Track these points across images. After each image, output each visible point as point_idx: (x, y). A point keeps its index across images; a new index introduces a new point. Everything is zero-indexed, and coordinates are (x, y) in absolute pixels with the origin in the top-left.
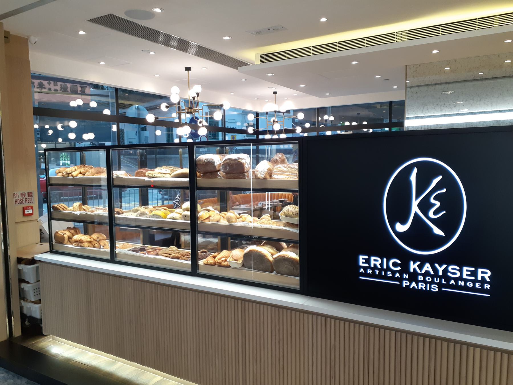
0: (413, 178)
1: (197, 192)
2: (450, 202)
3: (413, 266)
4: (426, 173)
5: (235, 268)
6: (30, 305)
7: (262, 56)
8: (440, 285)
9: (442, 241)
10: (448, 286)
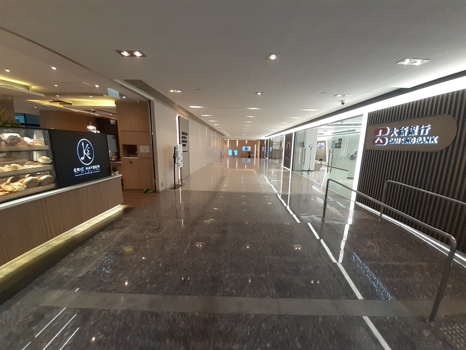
0: (83, 144)
3: (87, 168)
5: (21, 191)
9: (91, 160)
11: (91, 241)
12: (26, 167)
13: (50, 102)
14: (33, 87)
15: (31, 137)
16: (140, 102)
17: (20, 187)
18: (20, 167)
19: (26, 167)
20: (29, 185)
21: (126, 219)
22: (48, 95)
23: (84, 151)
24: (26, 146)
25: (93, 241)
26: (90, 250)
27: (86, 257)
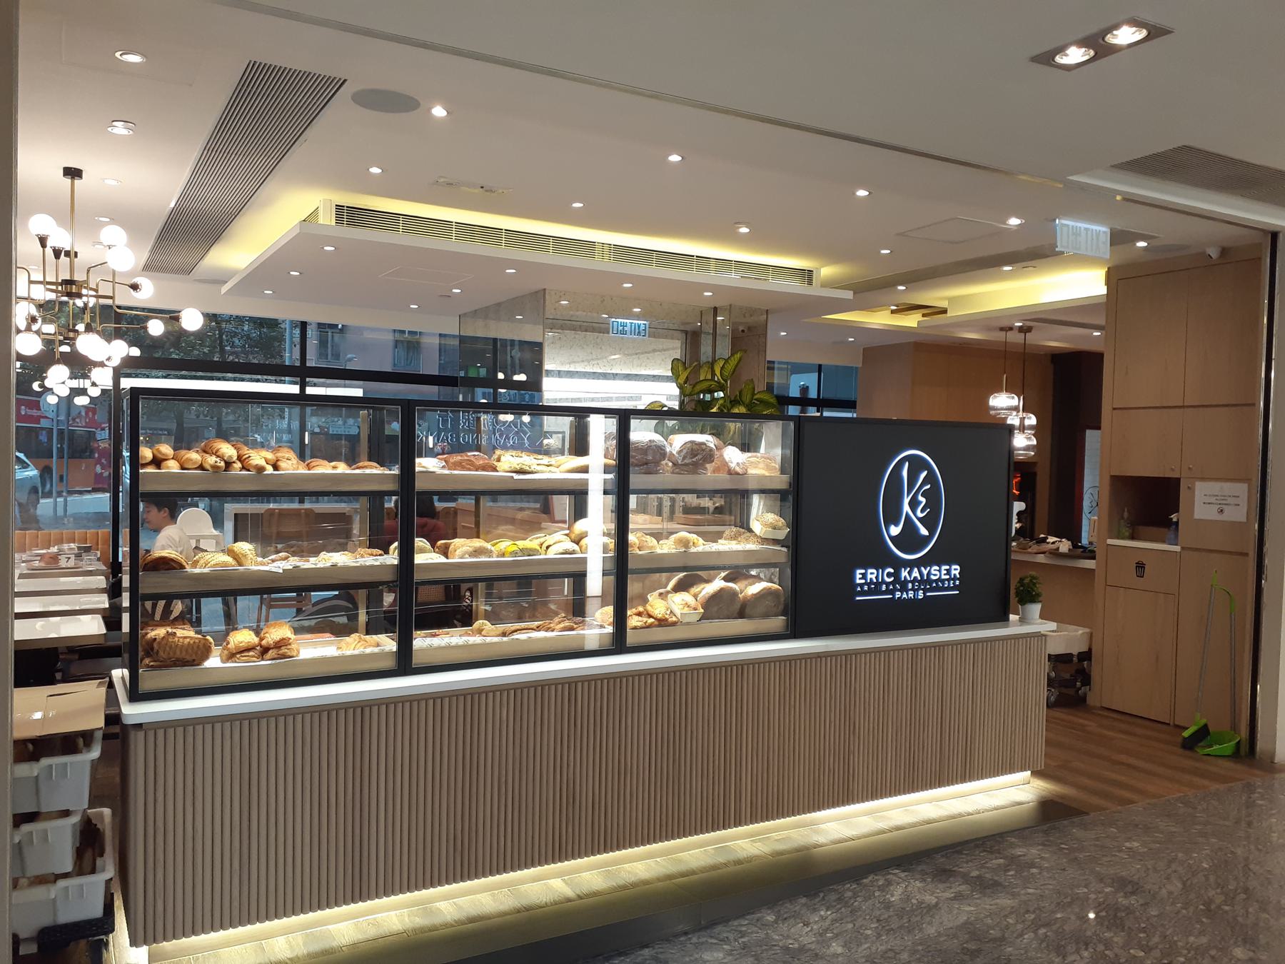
0: (905, 473)
3: (904, 573)
5: (688, 624)
7: (339, 208)
8: (925, 591)
10: (932, 590)
11: (849, 889)
12: (724, 545)
13: (893, 312)
14: (827, 271)
15: (747, 445)
16: (1224, 252)
17: (686, 610)
18: (701, 546)
19: (724, 545)
20: (717, 606)
21: (1019, 852)
22: (867, 291)
23: (906, 500)
24: (723, 476)
25: (855, 896)
26: (826, 930)
27: (802, 949)
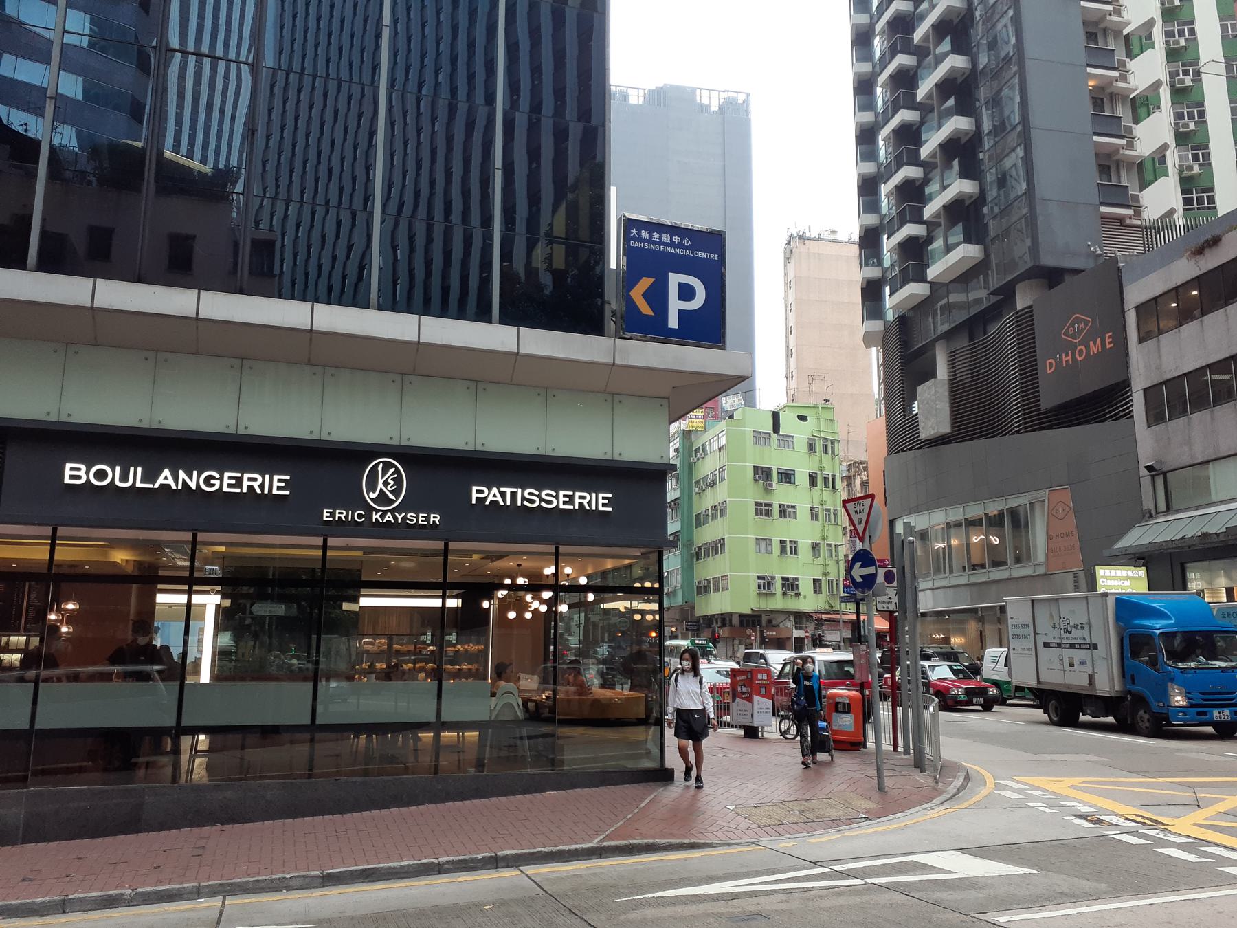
0: (380, 468)
1: (560, 558)
2: (398, 481)
3: (375, 516)
4: (387, 466)
6: (938, 178)
9: (393, 502)
